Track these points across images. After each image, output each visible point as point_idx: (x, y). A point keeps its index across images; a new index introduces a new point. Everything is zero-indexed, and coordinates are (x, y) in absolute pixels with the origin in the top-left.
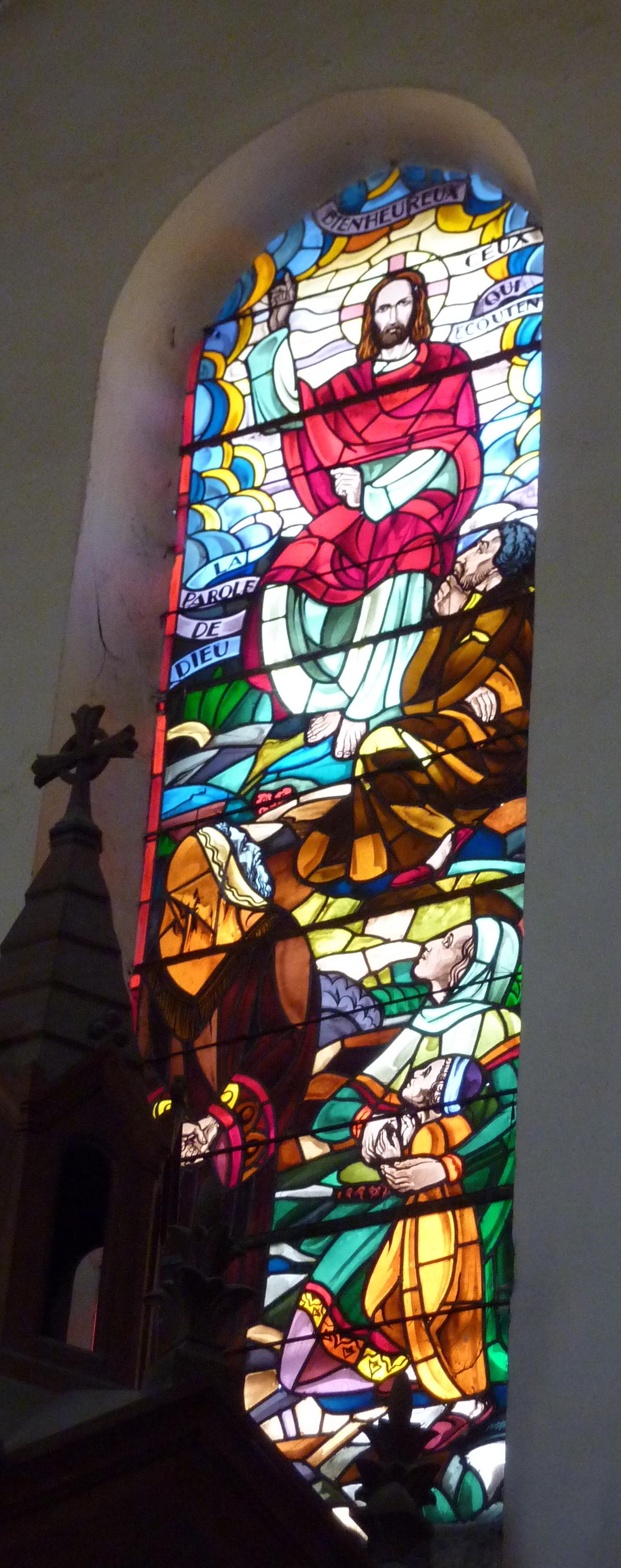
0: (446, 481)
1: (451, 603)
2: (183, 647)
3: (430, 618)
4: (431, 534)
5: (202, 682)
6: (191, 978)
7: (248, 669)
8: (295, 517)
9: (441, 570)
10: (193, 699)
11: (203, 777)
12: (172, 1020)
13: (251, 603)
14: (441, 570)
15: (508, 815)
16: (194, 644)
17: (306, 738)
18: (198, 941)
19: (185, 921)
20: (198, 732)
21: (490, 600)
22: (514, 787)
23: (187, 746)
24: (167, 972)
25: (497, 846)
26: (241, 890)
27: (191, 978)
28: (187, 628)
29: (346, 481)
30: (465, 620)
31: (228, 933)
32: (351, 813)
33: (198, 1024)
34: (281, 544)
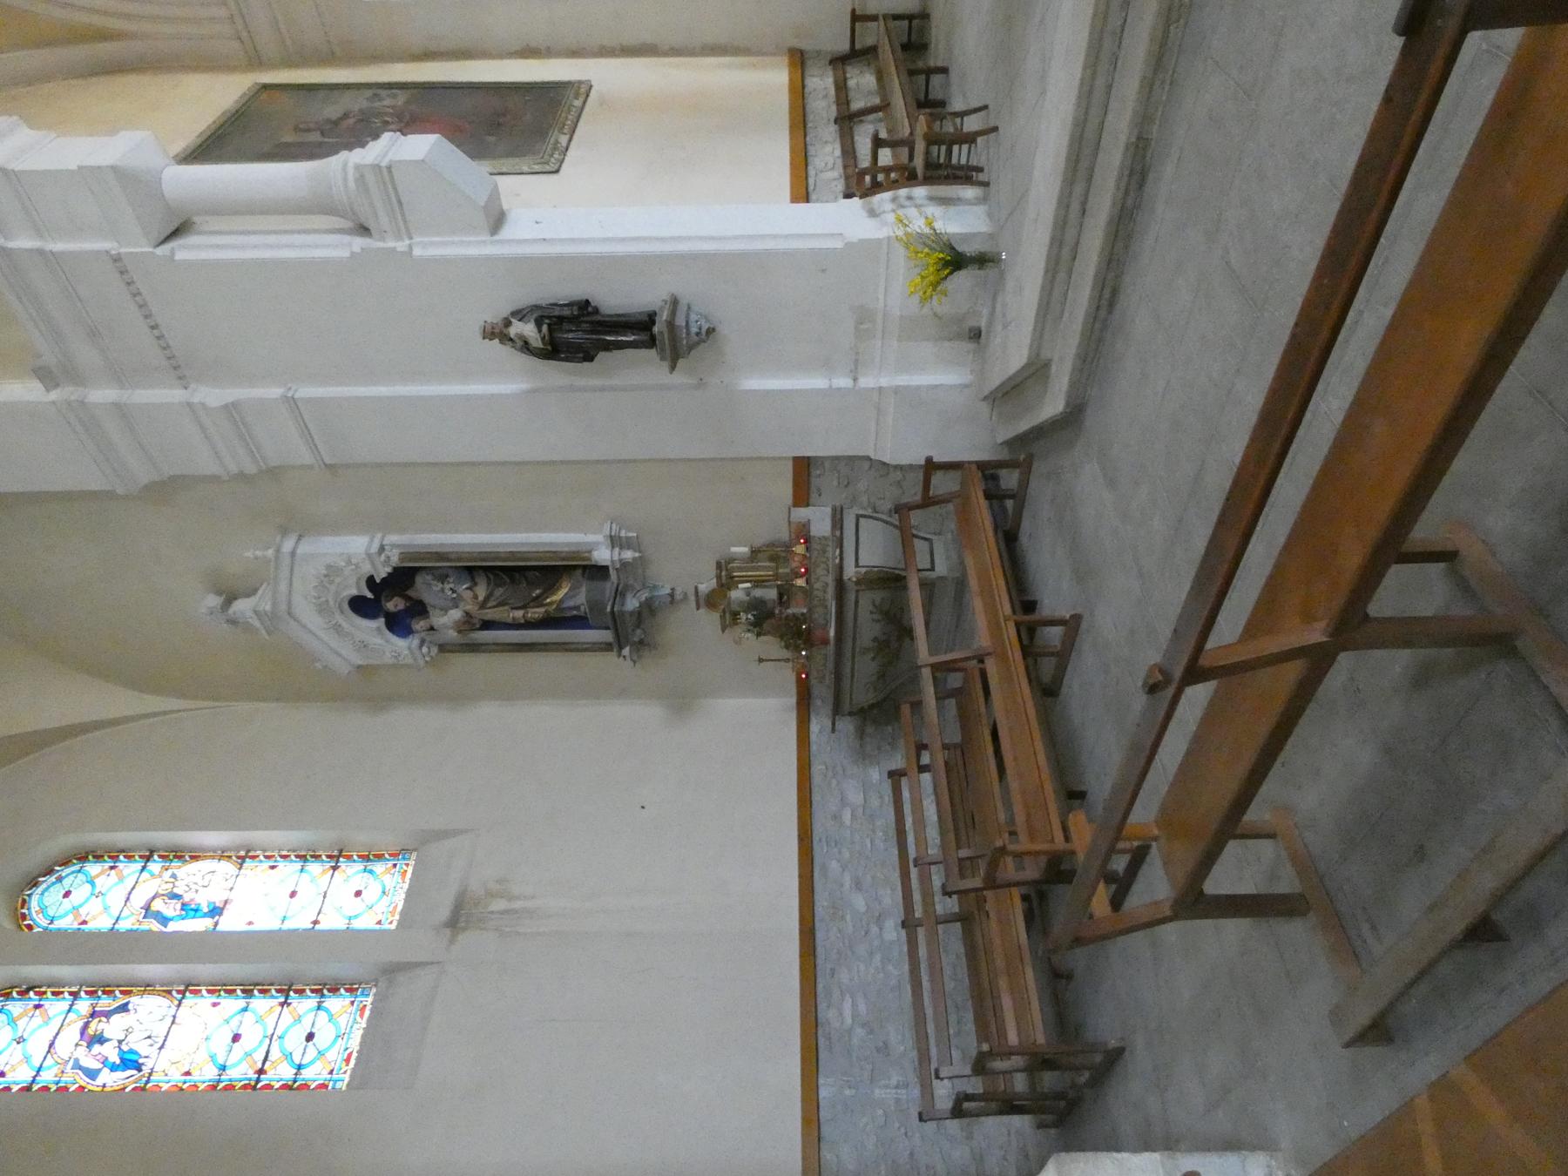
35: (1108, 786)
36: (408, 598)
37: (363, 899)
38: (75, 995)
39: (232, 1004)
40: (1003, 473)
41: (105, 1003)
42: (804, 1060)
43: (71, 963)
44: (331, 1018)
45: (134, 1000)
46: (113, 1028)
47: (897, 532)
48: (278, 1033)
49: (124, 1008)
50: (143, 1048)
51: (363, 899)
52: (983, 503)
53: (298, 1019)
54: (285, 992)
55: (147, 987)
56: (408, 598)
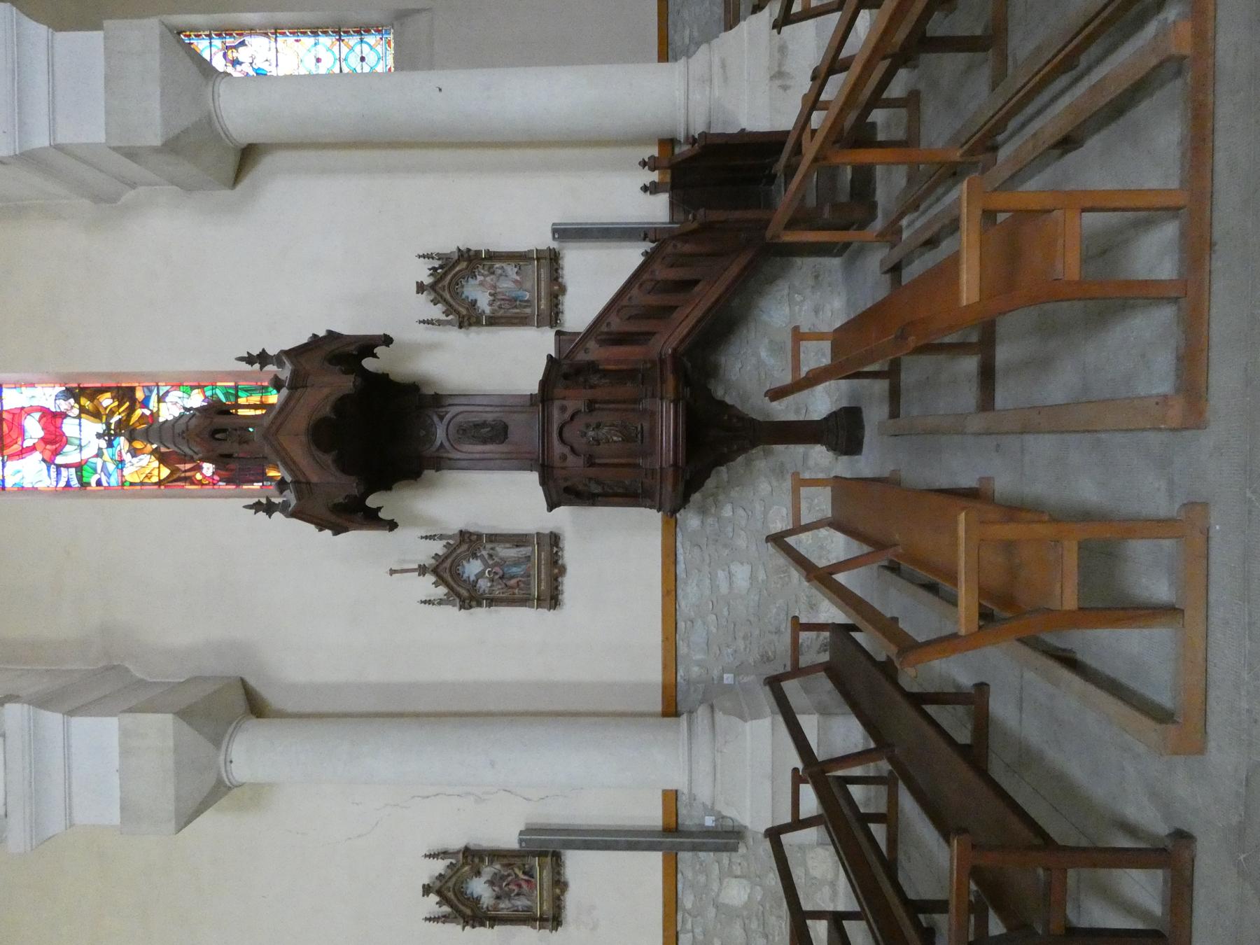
0: (37, 415)
1: (76, 412)
2: (68, 485)
3: (79, 417)
4: (52, 419)
5: (80, 478)
6: (165, 472)
7: (79, 467)
8: (37, 456)
9: (63, 415)
10: (85, 480)
11: (109, 475)
12: (175, 477)
13: (59, 467)
14: (63, 415)
15: (140, 395)
16: (68, 482)
17: (878, 818)
18: (156, 472)
19: (148, 476)
20: (96, 477)
21: (77, 401)
22: (132, 390)
23: (99, 483)
24: (995, 937)
25: (147, 398)
26: (144, 463)
27: (165, 472)
28: (62, 484)
29: (28, 443)
30: (83, 410)
31: (156, 463)
32: (783, 144)
33: (178, 469)
34: (44, 460)
35: (1031, 46)
36: (33, 449)
37: (241, 412)
38: (209, 36)
39: (308, 41)
40: (1140, 550)
41: (230, 41)
42: (665, 905)
43: (200, 12)
44: (371, 47)
45: (247, 39)
46: (242, 54)
47: (822, 563)
48: (343, 56)
49: (243, 44)
50: (265, 66)
51: (241, 412)
52: (1003, 154)
53: (352, 49)
54: (338, 33)
55: (252, 30)
56: (33, 449)
